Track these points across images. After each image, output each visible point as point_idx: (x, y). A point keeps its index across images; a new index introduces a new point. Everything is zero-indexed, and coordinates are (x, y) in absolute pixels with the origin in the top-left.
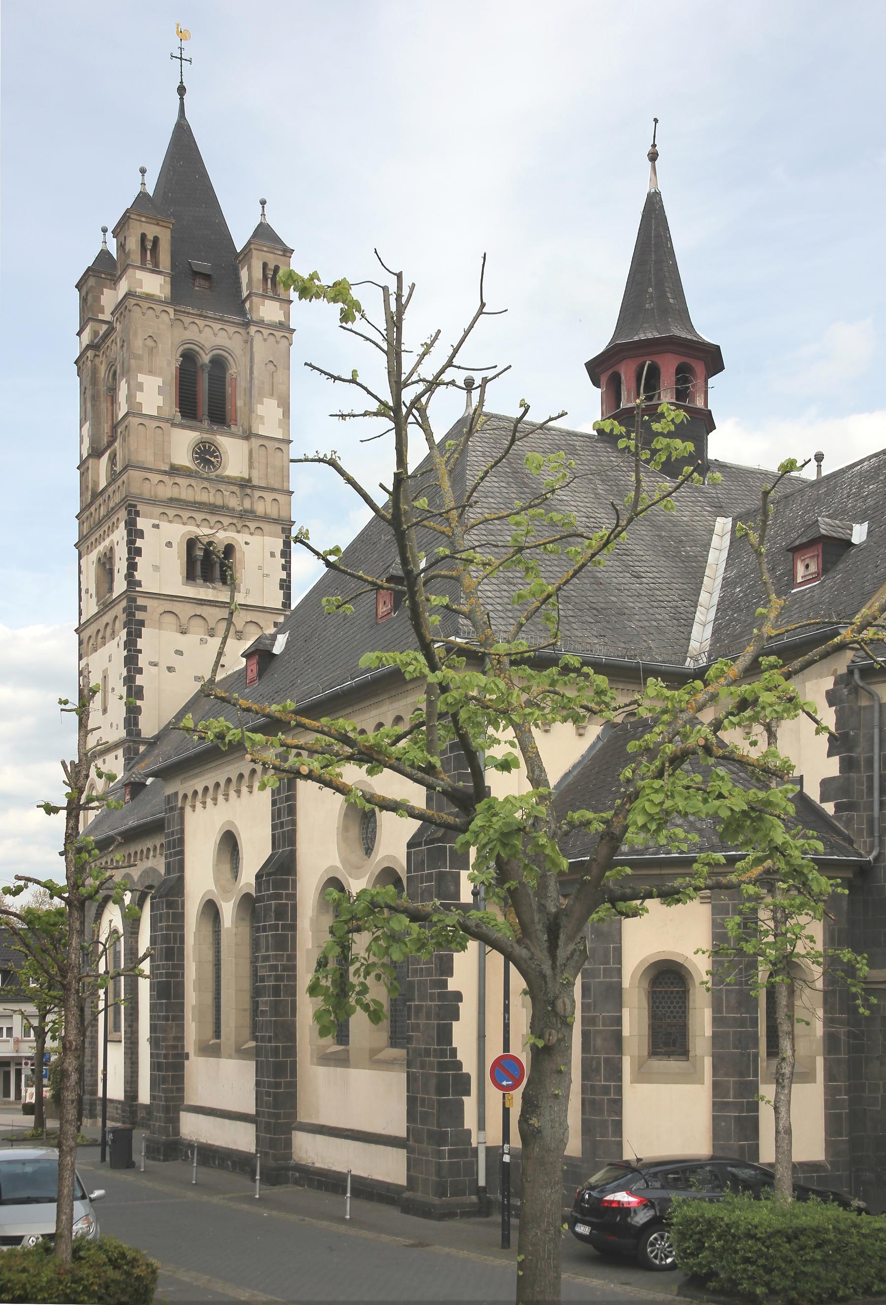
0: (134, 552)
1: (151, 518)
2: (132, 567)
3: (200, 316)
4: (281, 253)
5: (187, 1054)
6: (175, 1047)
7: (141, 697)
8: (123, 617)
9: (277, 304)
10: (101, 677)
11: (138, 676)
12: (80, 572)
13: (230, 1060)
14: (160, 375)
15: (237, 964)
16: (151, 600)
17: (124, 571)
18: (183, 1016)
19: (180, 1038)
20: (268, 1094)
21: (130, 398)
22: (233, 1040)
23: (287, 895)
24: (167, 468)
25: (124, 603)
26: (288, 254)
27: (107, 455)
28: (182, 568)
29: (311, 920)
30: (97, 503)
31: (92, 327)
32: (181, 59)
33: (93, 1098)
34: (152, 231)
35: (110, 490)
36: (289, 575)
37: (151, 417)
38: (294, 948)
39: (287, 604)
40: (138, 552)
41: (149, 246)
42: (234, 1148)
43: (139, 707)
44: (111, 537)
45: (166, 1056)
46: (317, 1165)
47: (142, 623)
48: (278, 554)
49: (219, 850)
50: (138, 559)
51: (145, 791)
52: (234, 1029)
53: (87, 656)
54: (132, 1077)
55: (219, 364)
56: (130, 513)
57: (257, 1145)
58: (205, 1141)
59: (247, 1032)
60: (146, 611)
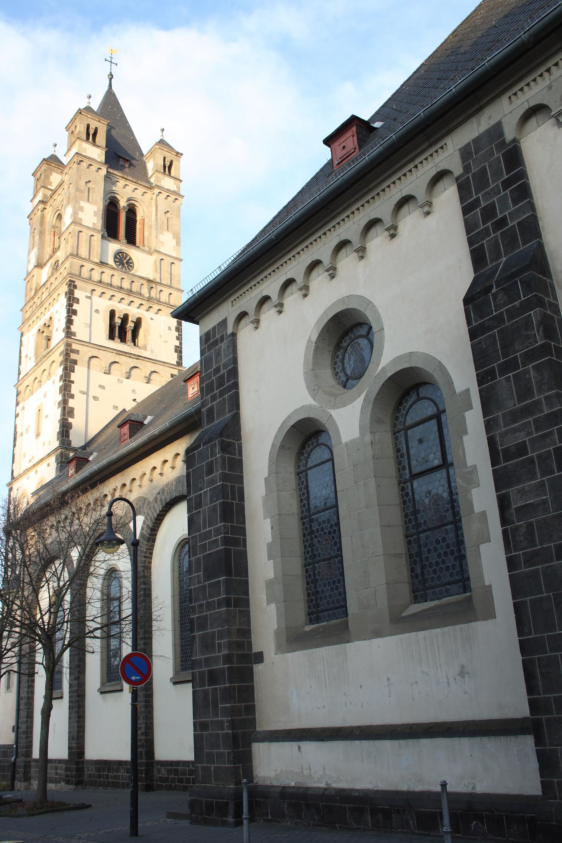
0: (71, 312)
2: (70, 322)
3: (123, 178)
6: (240, 645)
7: (72, 417)
8: (61, 358)
9: (172, 181)
10: (36, 410)
12: (21, 345)
14: (96, 205)
16: (82, 346)
18: (248, 600)
21: (75, 214)
24: (98, 261)
25: (62, 348)
26: (180, 156)
27: (48, 265)
31: (43, 192)
32: (111, 62)
33: (28, 759)
34: (94, 124)
35: (52, 279)
36: (181, 344)
37: (88, 228)
39: (179, 363)
40: (75, 312)
41: (92, 132)
44: (50, 311)
47: (75, 362)
48: (173, 329)
49: (317, 349)
50: (74, 317)
51: (89, 463)
53: (24, 400)
54: (79, 732)
55: (131, 212)
56: (70, 286)
58: (322, 785)
60: (78, 354)
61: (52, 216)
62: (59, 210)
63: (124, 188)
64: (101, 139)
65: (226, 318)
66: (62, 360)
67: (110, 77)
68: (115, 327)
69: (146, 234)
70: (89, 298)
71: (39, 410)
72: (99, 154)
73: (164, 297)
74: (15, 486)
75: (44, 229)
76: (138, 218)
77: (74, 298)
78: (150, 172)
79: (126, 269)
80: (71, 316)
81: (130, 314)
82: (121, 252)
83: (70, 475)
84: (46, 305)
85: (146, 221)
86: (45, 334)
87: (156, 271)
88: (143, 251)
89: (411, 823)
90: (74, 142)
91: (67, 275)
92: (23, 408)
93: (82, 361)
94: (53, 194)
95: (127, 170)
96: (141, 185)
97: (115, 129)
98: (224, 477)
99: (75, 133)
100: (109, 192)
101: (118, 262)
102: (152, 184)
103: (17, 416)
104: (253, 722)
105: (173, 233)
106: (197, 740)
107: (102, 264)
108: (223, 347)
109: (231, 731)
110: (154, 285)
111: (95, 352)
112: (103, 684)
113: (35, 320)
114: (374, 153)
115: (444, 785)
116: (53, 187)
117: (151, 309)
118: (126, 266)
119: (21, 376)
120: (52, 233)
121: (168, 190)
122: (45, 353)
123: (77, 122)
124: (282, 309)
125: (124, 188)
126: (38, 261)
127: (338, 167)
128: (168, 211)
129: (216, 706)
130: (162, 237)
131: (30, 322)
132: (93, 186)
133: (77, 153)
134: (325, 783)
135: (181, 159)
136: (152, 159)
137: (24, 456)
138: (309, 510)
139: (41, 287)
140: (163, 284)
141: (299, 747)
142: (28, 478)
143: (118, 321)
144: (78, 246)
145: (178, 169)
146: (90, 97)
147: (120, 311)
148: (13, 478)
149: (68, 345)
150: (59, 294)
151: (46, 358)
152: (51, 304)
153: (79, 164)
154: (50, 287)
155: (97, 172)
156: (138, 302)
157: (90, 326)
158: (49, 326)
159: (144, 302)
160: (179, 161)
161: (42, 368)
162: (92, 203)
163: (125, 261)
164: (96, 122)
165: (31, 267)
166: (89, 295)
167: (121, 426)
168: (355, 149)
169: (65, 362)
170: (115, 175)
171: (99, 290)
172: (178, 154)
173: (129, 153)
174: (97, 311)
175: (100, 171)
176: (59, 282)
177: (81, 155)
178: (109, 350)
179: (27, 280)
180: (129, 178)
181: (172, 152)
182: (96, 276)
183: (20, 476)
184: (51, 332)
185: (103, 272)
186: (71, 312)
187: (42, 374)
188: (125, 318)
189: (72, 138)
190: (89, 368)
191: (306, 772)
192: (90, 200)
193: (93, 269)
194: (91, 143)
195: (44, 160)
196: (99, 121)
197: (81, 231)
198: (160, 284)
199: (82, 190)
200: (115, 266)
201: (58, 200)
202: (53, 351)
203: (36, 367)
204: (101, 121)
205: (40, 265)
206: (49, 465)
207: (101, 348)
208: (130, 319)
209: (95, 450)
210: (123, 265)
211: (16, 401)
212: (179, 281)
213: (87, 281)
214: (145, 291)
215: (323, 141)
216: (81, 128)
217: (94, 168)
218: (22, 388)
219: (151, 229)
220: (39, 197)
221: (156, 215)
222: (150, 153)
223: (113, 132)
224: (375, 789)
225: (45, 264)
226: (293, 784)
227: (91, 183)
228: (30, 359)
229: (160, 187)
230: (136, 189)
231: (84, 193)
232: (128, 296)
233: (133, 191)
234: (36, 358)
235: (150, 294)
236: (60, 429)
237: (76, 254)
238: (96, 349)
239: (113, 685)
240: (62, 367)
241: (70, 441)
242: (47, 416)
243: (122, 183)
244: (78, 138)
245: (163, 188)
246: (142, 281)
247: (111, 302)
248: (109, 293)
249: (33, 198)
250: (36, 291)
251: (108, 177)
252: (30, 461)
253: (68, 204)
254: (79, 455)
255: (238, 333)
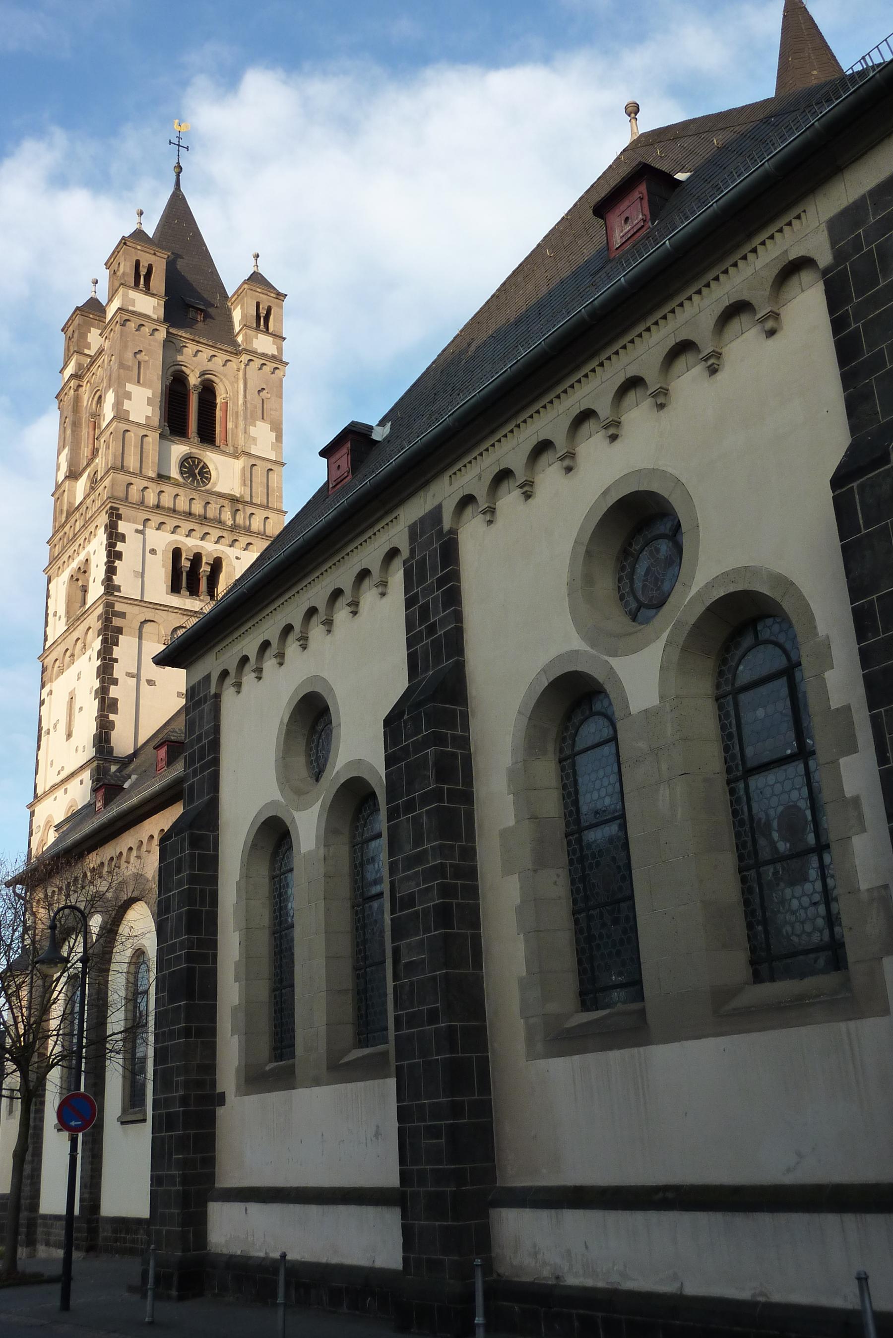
1: (133, 523)
2: (111, 570)
4: (274, 296)
5: (222, 1096)
7: (115, 712)
8: (99, 625)
9: (270, 339)
10: (67, 699)
11: (112, 687)
12: (48, 596)
13: (316, 1090)
14: (150, 387)
15: (327, 910)
16: (130, 606)
17: (102, 576)
19: (209, 1068)
20: (433, 1132)
21: (118, 405)
22: (322, 1046)
23: (454, 738)
25: (100, 610)
26: (282, 298)
27: (85, 475)
28: (166, 576)
29: (512, 774)
30: (73, 520)
31: (76, 360)
32: (179, 145)
35: (89, 501)
37: (139, 425)
38: (471, 837)
40: (119, 556)
41: (143, 272)
42: (335, 1260)
43: (113, 723)
44: (86, 550)
45: (184, 1101)
46: (572, 1280)
47: (119, 631)
50: (117, 563)
52: (323, 1029)
53: (51, 681)
55: (208, 391)
56: (111, 515)
57: (407, 1245)
58: (262, 1254)
59: (348, 1032)
60: (125, 618)
61: (91, 399)
62: (99, 390)
63: (195, 356)
64: (158, 282)
65: (210, 673)
66: (100, 627)
67: (177, 170)
68: (182, 573)
69: (230, 425)
70: (142, 532)
71: (72, 698)
72: (154, 307)
73: (256, 524)
74: (38, 809)
75: (80, 419)
76: (219, 400)
77: (117, 534)
78: (237, 328)
79: (198, 482)
80: (114, 562)
81: (203, 553)
82: (190, 458)
83: (97, 810)
84: (80, 541)
85: (230, 405)
86: (80, 583)
87: (245, 485)
88: (224, 453)
89: (324, 1298)
90: (117, 290)
91: (107, 499)
92: (51, 693)
93: (130, 627)
94: (91, 366)
95: (200, 325)
96: (221, 349)
97: (183, 258)
98: (192, 879)
99: (118, 274)
100: (172, 364)
101: (186, 473)
102: (240, 346)
103: (42, 703)
104: (211, 1177)
105: (271, 423)
106: (153, 1195)
107: (162, 477)
108: (206, 708)
109: (181, 1188)
110: (240, 507)
111: (149, 614)
112: (124, 1111)
113: (66, 561)
114: (330, 517)
115: (283, 1256)
116: (92, 352)
117: (237, 542)
118: (199, 478)
119: (48, 644)
120: (91, 425)
121: (263, 355)
122: (79, 613)
123: (121, 257)
124: (261, 674)
125: (195, 356)
126: (70, 469)
127: (332, 491)
128: (263, 389)
129: (170, 1155)
130: (253, 431)
131: (60, 562)
132: (147, 358)
133: (119, 309)
134: (264, 1252)
135: (284, 303)
136: (239, 307)
137: (52, 765)
138: (578, 821)
139: (73, 512)
140: (255, 504)
141: (246, 1209)
142: (55, 799)
143: (186, 564)
144: (123, 453)
145: (280, 321)
146: (141, 213)
147: (189, 549)
148: (36, 796)
149: (109, 606)
150: (97, 526)
151: (80, 622)
152: (93, 534)
153: (123, 325)
154: (86, 513)
155: (151, 335)
156: (215, 533)
157: (143, 575)
158: (85, 572)
159: (225, 534)
160: (281, 307)
161: (75, 635)
162: (144, 385)
163: (197, 471)
164: (151, 256)
165: (61, 477)
166: (141, 527)
167: (156, 748)
168: (349, 472)
169: (105, 631)
170: (181, 336)
171: (156, 519)
172: (281, 296)
173: (205, 296)
174: (153, 552)
175: (156, 333)
176: (97, 508)
177: (127, 311)
178: (170, 610)
179: (56, 496)
180: (202, 341)
181: (269, 294)
182: (151, 498)
183: (46, 794)
184: (88, 581)
185: (162, 492)
186: (113, 556)
187: (76, 644)
188: (197, 559)
189: (115, 281)
190: (140, 638)
191: (250, 1239)
192: (141, 382)
193: (146, 488)
194: (142, 291)
195: (78, 308)
196: (155, 254)
197: (128, 431)
198: (251, 503)
199: (129, 366)
200: (181, 479)
201: (98, 374)
202: (90, 611)
203: (68, 634)
204: (158, 254)
205: (73, 475)
206: (81, 782)
207: (159, 607)
208: (204, 561)
209: (134, 771)
210: (194, 476)
211: (42, 681)
212: (280, 497)
213: (138, 507)
214: (227, 516)
215: (319, 453)
216: (126, 267)
217: (146, 330)
218: (49, 661)
219: (237, 417)
220: (70, 370)
221: (245, 397)
222: (236, 296)
223: (180, 264)
224: (303, 1260)
225: (81, 474)
226: (239, 1253)
227: (143, 353)
228: (60, 618)
229: (250, 351)
230: (215, 356)
231: (132, 371)
232: (200, 525)
233: (209, 360)
234: (68, 618)
235: (234, 520)
236: (96, 731)
237: (120, 467)
238: (150, 610)
239: (136, 1113)
240: (101, 637)
241: (112, 748)
242: (81, 709)
243: (191, 348)
244: (122, 284)
245: (256, 353)
246: (222, 501)
247: (174, 537)
248: (171, 523)
249: (63, 368)
250: (69, 514)
251: (170, 344)
252: (59, 773)
253: (110, 387)
254: (109, 780)
255: (223, 693)
